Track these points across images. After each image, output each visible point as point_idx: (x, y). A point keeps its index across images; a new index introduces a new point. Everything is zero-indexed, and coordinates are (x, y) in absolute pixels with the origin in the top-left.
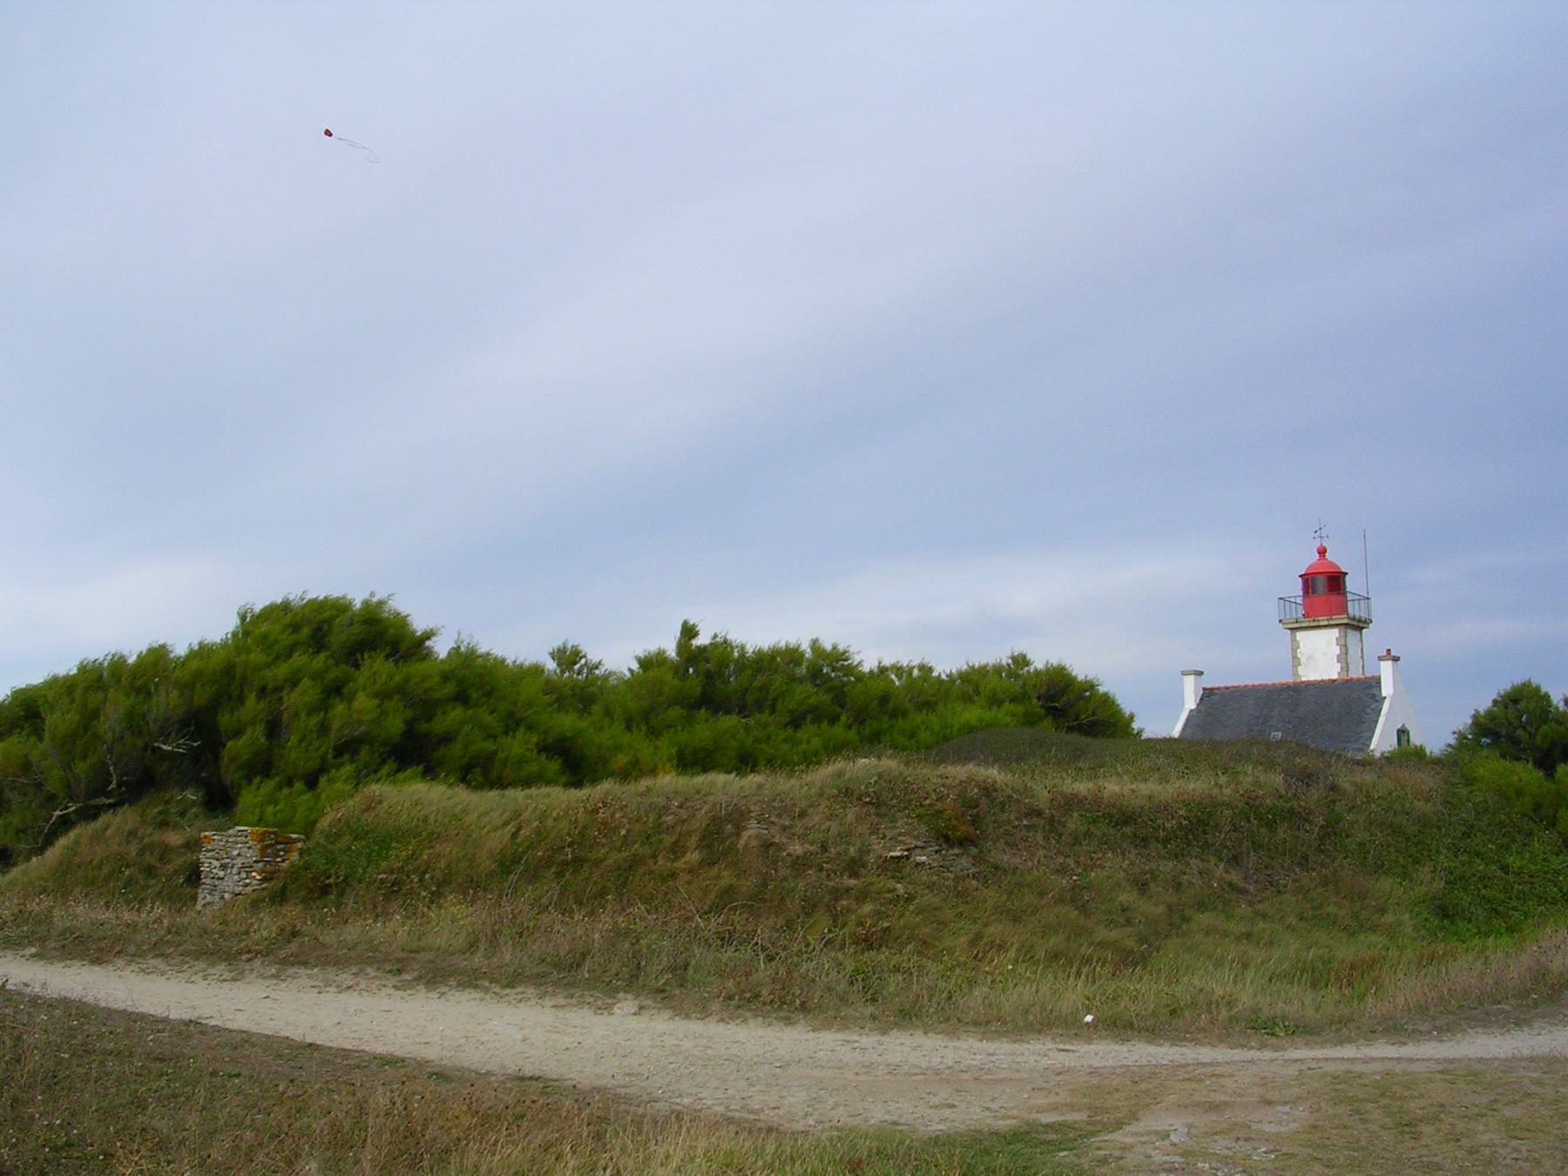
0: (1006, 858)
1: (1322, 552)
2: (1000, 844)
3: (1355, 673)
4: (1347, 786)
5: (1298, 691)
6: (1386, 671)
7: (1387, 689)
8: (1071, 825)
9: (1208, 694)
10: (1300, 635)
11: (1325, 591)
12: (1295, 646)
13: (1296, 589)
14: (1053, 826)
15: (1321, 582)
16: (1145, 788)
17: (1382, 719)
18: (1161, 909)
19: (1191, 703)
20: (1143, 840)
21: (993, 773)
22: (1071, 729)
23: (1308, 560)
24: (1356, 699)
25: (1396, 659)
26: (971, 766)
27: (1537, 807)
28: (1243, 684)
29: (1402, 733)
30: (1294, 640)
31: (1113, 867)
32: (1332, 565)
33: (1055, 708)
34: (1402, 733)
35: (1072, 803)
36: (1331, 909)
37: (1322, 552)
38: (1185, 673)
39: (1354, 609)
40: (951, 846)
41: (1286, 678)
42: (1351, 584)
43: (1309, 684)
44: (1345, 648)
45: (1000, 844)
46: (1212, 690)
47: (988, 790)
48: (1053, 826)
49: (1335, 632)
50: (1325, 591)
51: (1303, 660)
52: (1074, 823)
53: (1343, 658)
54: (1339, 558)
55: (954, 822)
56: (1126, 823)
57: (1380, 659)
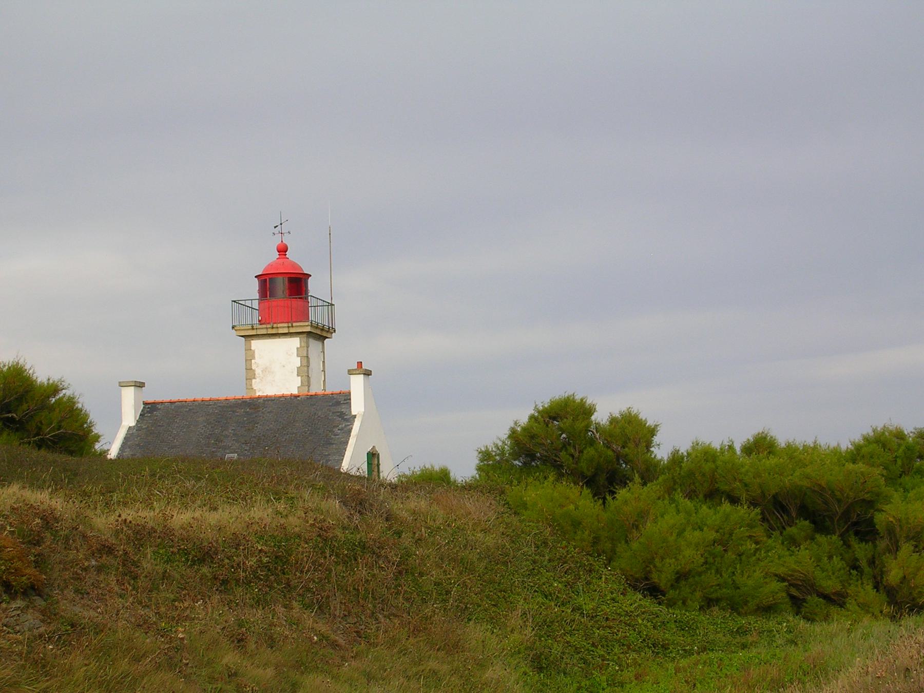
0: (77, 609)
1: (283, 250)
2: (70, 593)
3: (317, 388)
4: (404, 514)
5: (254, 407)
6: (357, 386)
7: (357, 406)
8: (146, 565)
9: (149, 409)
10: (256, 344)
11: (285, 294)
12: (249, 356)
13: (252, 290)
14: (130, 571)
15: (281, 285)
16: (213, 518)
17: (352, 441)
18: (270, 672)
19: (129, 419)
20: (225, 582)
21: (41, 498)
22: (40, 445)
23: (266, 259)
24: (320, 417)
25: (367, 373)
26: (14, 488)
27: (596, 541)
28: (190, 398)
29: (373, 456)
30: (248, 349)
31: (208, 616)
32: (294, 265)
33: (12, 420)
34: (373, 456)
35: (140, 535)
36: (432, 664)
37: (283, 250)
38: (122, 385)
39: (317, 315)
40: (13, 597)
41: (236, 392)
42: (314, 287)
43: (268, 400)
44: (306, 360)
45: (70, 593)
46: (154, 404)
47: (49, 520)
48: (130, 571)
49: (295, 342)
50: (285, 294)
51: (258, 371)
52: (149, 562)
53: (305, 371)
54: (300, 258)
55: (19, 564)
56: (202, 561)
57: (351, 372)
